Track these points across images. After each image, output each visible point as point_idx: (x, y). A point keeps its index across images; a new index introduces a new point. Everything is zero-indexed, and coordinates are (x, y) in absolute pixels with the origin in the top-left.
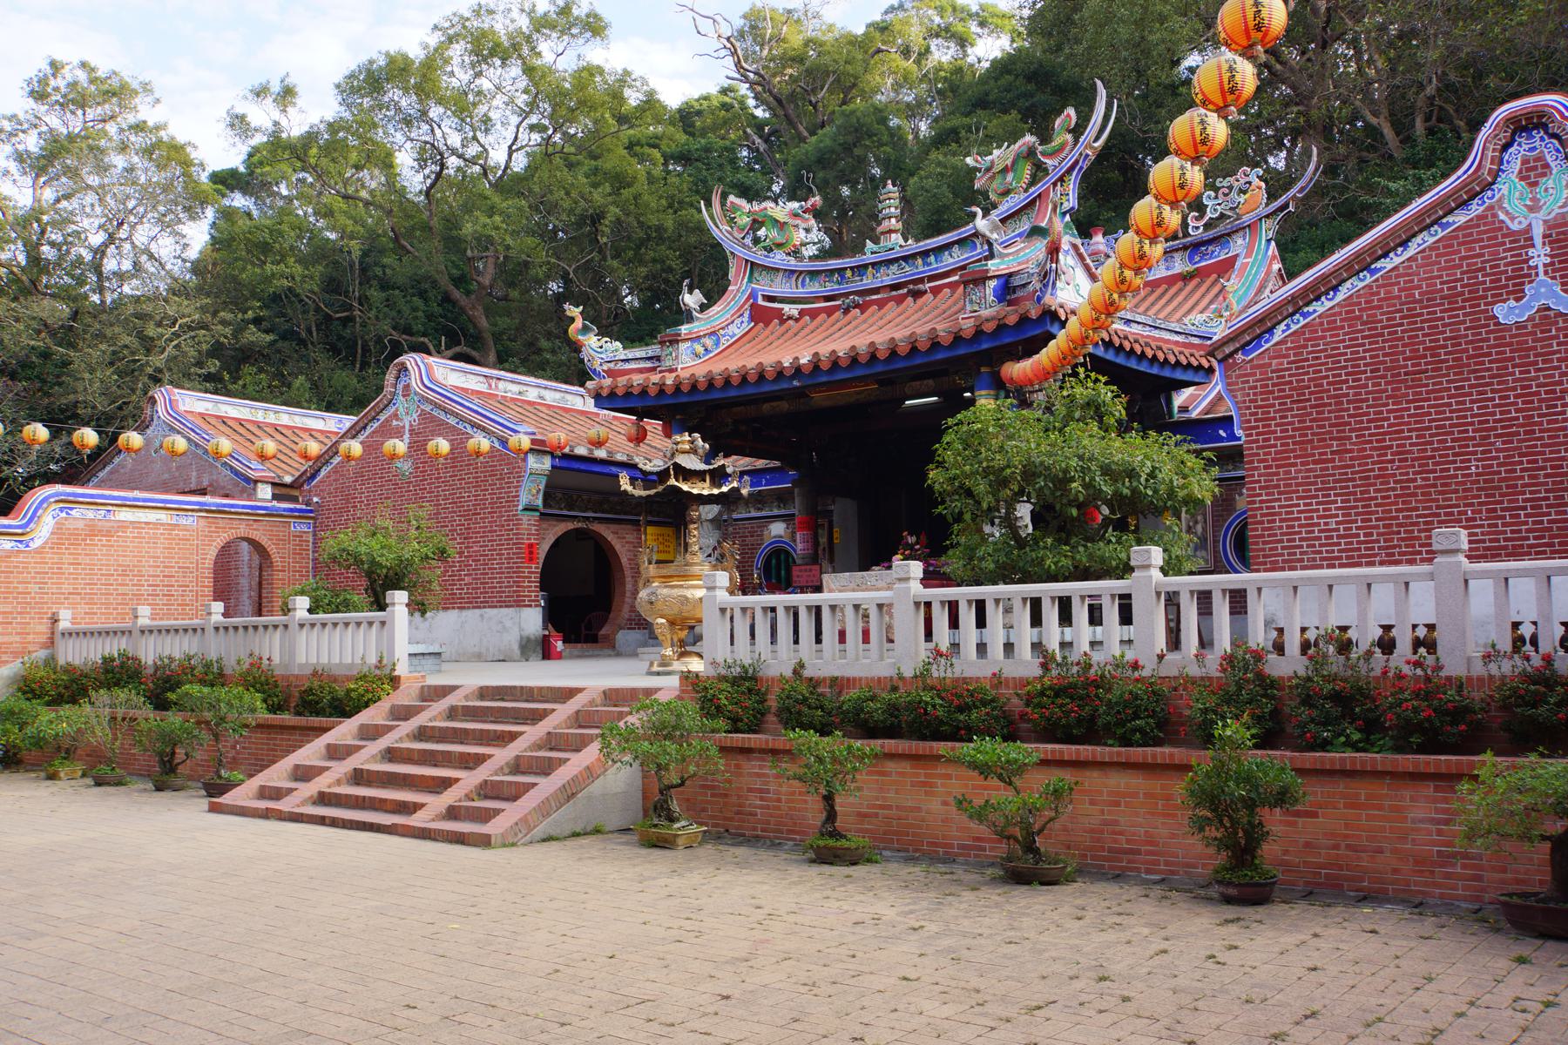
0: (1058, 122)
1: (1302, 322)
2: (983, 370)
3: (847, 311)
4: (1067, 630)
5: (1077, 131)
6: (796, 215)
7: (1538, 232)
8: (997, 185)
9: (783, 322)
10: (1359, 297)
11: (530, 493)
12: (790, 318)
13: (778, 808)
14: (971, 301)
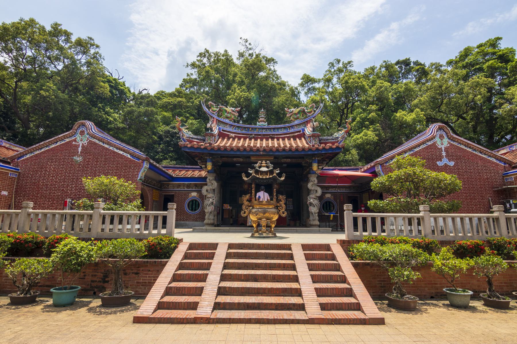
4: (419, 227)
7: (443, 149)
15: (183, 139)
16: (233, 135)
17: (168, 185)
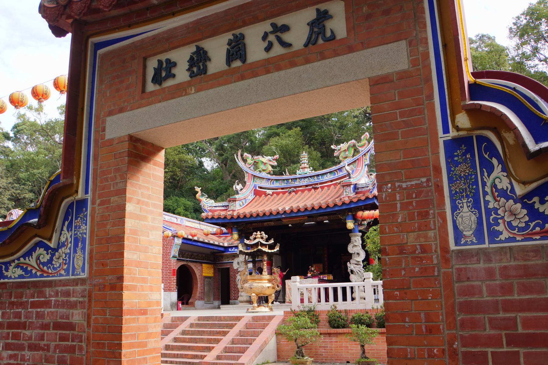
0: (363, 137)
3: (290, 193)
6: (270, 161)
8: (343, 154)
12: (269, 194)
13: (332, 352)
14: (346, 192)
16: (270, 192)
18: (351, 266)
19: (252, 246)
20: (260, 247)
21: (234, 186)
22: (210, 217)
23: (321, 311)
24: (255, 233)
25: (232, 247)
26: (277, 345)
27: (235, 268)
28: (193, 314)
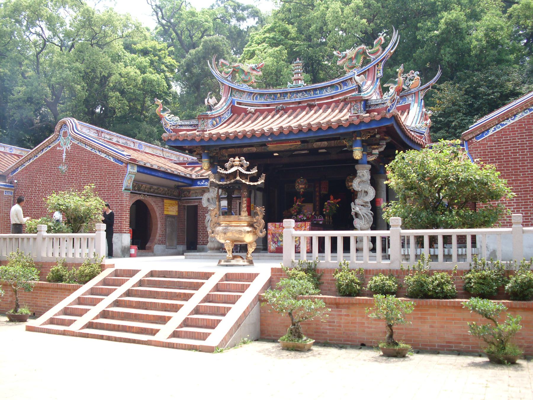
1: (501, 128)
2: (358, 138)
5: (384, 46)
9: (247, 114)
10: (524, 119)
11: (127, 182)
12: (250, 112)
13: (340, 330)
15: (167, 129)
16: (252, 109)
17: (189, 191)
18: (356, 208)
19: (228, 176)
20: (238, 178)
21: (206, 100)
22: (173, 139)
23: (324, 270)
24: (232, 159)
25: (201, 180)
26: (261, 316)
27: (205, 206)
28: (145, 264)
